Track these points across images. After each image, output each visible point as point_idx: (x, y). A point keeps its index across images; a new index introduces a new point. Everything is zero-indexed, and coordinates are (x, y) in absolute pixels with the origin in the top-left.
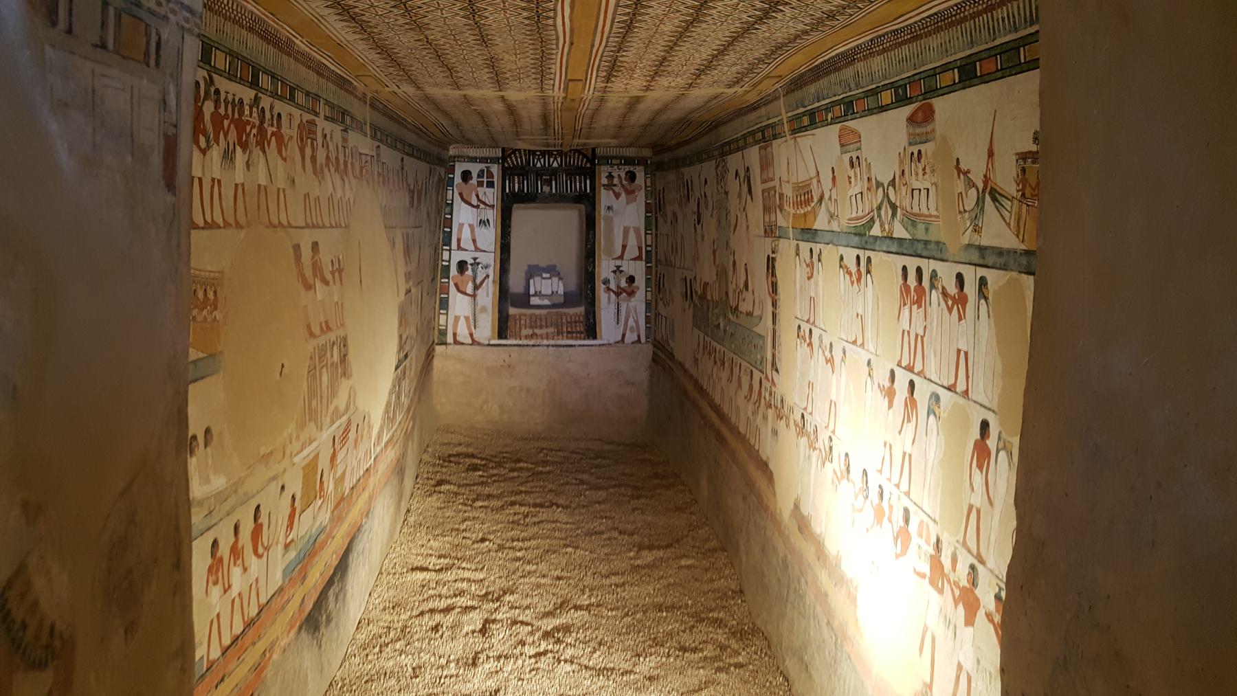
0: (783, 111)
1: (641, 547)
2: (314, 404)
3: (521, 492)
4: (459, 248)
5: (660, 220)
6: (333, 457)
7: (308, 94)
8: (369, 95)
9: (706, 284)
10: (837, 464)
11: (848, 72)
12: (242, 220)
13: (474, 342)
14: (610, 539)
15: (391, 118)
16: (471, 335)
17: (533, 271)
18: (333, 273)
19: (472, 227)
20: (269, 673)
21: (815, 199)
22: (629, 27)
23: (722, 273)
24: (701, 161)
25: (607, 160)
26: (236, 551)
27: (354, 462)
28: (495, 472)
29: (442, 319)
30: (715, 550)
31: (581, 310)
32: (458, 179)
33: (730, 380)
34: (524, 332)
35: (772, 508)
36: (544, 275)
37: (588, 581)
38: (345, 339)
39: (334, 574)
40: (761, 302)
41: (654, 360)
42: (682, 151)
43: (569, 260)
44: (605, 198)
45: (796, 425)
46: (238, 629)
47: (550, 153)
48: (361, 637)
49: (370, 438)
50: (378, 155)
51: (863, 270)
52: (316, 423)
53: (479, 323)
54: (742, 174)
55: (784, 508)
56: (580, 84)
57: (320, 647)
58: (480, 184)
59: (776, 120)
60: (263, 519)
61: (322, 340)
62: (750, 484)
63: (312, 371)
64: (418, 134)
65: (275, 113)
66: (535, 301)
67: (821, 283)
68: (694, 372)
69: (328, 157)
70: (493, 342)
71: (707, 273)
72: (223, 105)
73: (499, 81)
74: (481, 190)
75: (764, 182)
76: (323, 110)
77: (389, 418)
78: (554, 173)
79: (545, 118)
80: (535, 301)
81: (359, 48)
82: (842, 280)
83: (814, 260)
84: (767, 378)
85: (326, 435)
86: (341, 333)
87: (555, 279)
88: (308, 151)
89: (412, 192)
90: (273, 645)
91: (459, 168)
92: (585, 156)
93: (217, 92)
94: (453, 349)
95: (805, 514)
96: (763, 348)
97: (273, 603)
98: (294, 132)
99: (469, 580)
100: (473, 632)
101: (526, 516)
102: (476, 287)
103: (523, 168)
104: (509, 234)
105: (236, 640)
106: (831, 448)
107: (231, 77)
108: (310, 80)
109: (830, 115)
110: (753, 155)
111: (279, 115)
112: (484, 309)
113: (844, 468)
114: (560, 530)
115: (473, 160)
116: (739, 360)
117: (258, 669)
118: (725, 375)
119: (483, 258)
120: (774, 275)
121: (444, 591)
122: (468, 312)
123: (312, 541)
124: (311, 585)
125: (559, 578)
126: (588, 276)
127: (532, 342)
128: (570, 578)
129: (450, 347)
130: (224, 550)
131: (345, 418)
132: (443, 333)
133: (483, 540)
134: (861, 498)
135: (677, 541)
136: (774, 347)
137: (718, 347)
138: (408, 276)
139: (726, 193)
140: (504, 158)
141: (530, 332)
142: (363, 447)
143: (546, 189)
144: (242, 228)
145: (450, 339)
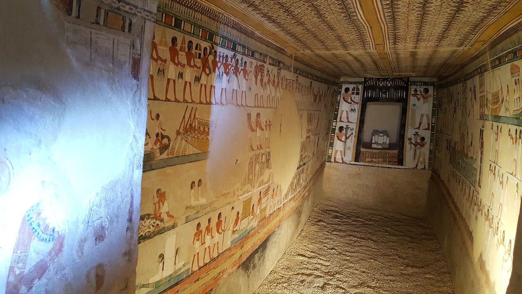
0: (489, 58)
1: (408, 265)
2: (251, 177)
3: (356, 231)
4: (341, 121)
5: (440, 112)
6: (260, 200)
7: (261, 54)
8: (294, 55)
9: (456, 142)
10: (499, 236)
11: (515, 37)
12: (224, 102)
13: (343, 162)
14: (393, 259)
15: (306, 65)
16: (342, 159)
17: (376, 132)
18: (266, 126)
19: (348, 112)
20: (221, 281)
21: (500, 101)
22: (394, 19)
23: (462, 137)
24: (457, 84)
25: (415, 83)
26: (208, 229)
27: (271, 205)
28: (346, 220)
29: (330, 151)
30: (445, 273)
31: (396, 152)
32: (343, 91)
33: (461, 190)
34: (367, 160)
35: (471, 255)
36: (380, 135)
37: (377, 276)
38: (269, 153)
39: (259, 248)
40: (477, 152)
41: (431, 178)
42: (450, 79)
43: (393, 127)
44: (412, 100)
45: (485, 215)
46: (207, 260)
47: (386, 79)
48: (271, 278)
49: (281, 195)
50: (297, 80)
51: (518, 137)
52: (251, 185)
53: (346, 154)
54: (472, 89)
55: (476, 256)
56: (382, 46)
57: (249, 277)
58: (353, 93)
59: (486, 62)
60: (223, 218)
61: (257, 152)
62: (464, 243)
63: (251, 163)
64: (322, 72)
65: (244, 61)
66: (374, 146)
67: (501, 144)
68: (447, 185)
69: (269, 80)
70: (352, 163)
71: (456, 138)
72: (218, 57)
73: (345, 46)
74: (353, 96)
75: (481, 93)
76: (268, 61)
77: (292, 188)
78: (388, 89)
79: (375, 62)
80: (374, 146)
81: (282, 34)
82: (509, 141)
83: (499, 130)
84: (476, 190)
85: (256, 191)
86: (268, 150)
87: (385, 137)
88: (259, 77)
89: (315, 97)
90: (224, 271)
91: (344, 87)
92: (404, 81)
93: (215, 52)
94: (333, 164)
95: (484, 260)
96: (476, 175)
97: (225, 254)
98: (253, 69)
99: (322, 264)
100: (318, 287)
101: (355, 242)
102: (347, 138)
103: (373, 86)
104: (364, 115)
105: (206, 265)
106: (498, 227)
107: (223, 46)
108: (264, 49)
109: (507, 59)
110: (477, 78)
111: (246, 62)
112: (349, 148)
113: (502, 238)
114: (370, 251)
115: (351, 83)
116: (466, 181)
117: (216, 279)
118: (460, 188)
119: (351, 126)
120: (482, 139)
121: (310, 267)
122: (342, 149)
123: (247, 232)
124: (246, 250)
125: (364, 272)
126: (402, 136)
127: (370, 165)
128: (369, 273)
129: (332, 163)
130: (203, 228)
131: (267, 185)
132: (330, 157)
133: (332, 249)
134: (507, 255)
135: (427, 265)
136: (480, 175)
137: (458, 173)
138: (308, 131)
139: (466, 98)
140: (365, 82)
141: (370, 160)
142: (276, 199)
143: (384, 96)
144: (223, 105)
145: (333, 160)
